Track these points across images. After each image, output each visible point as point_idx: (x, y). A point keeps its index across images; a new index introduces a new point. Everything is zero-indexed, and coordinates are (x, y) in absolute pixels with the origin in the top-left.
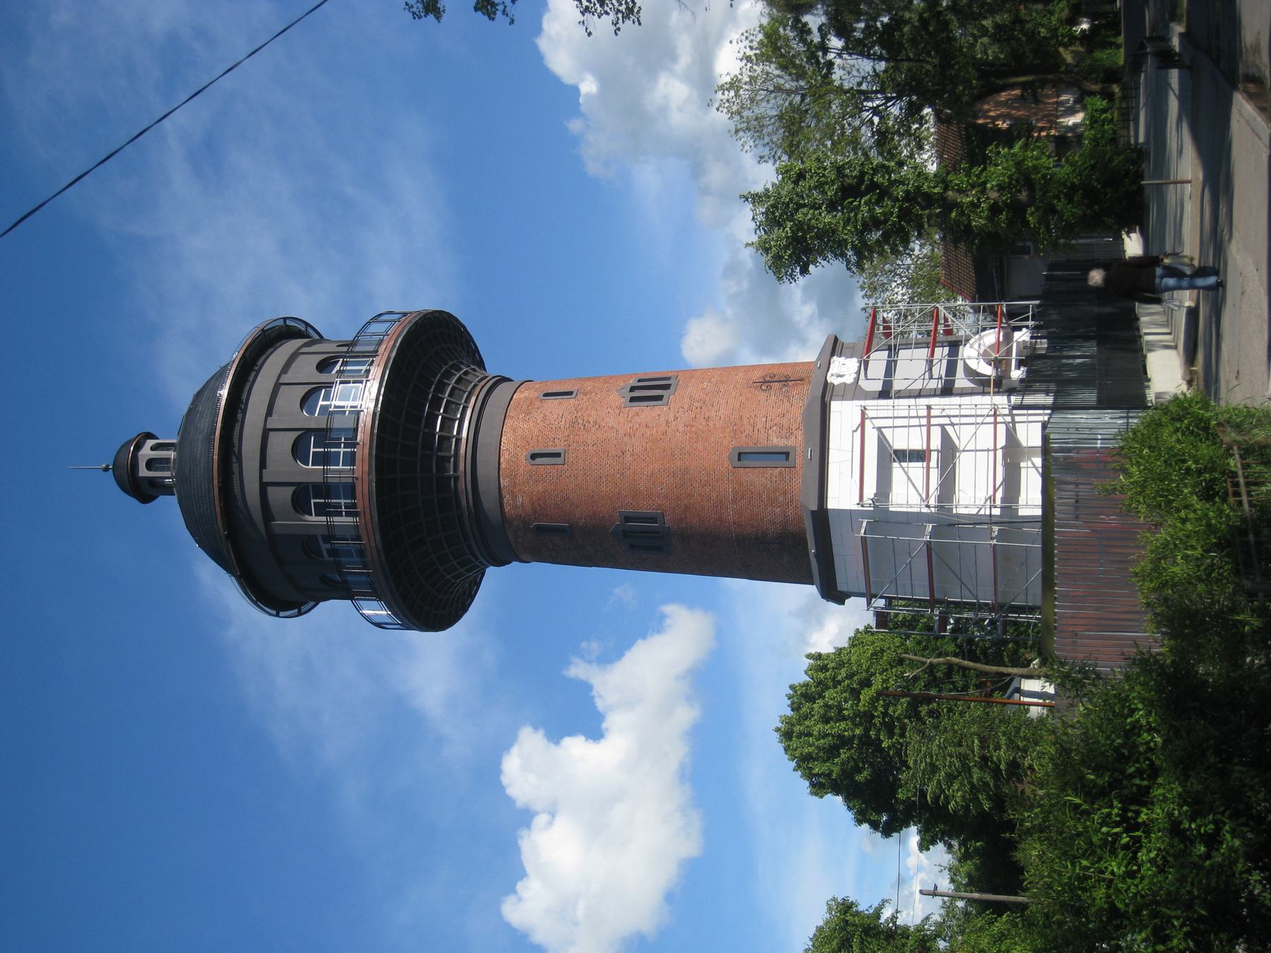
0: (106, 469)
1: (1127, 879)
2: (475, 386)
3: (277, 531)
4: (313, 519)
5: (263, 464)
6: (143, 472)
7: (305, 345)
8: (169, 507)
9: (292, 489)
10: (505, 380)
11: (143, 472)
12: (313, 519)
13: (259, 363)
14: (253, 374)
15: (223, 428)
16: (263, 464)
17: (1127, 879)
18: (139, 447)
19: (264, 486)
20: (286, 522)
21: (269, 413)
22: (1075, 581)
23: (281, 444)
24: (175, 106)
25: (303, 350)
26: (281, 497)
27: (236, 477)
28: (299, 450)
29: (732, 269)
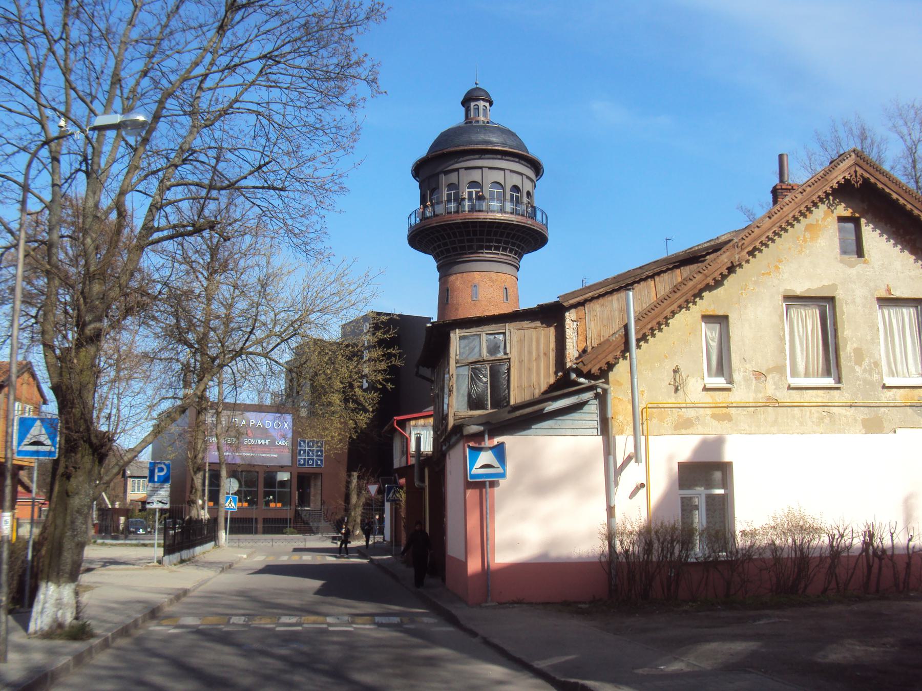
0: (476, 84)
1: (167, 485)
3: (440, 176)
4: (445, 193)
5: (467, 168)
6: (472, 104)
7: (528, 178)
8: (455, 117)
9: (457, 183)
10: (518, 270)
11: (472, 104)
12: (445, 193)
13: (507, 158)
14: (517, 160)
15: (498, 150)
16: (467, 168)
17: (167, 485)
18: (483, 100)
19: (457, 170)
20: (444, 180)
21: (512, 171)
22: (545, 354)
23: (476, 176)
24: (820, 392)
25: (524, 177)
26: (453, 178)
27: (472, 157)
28: (473, 184)
29: (463, 394)
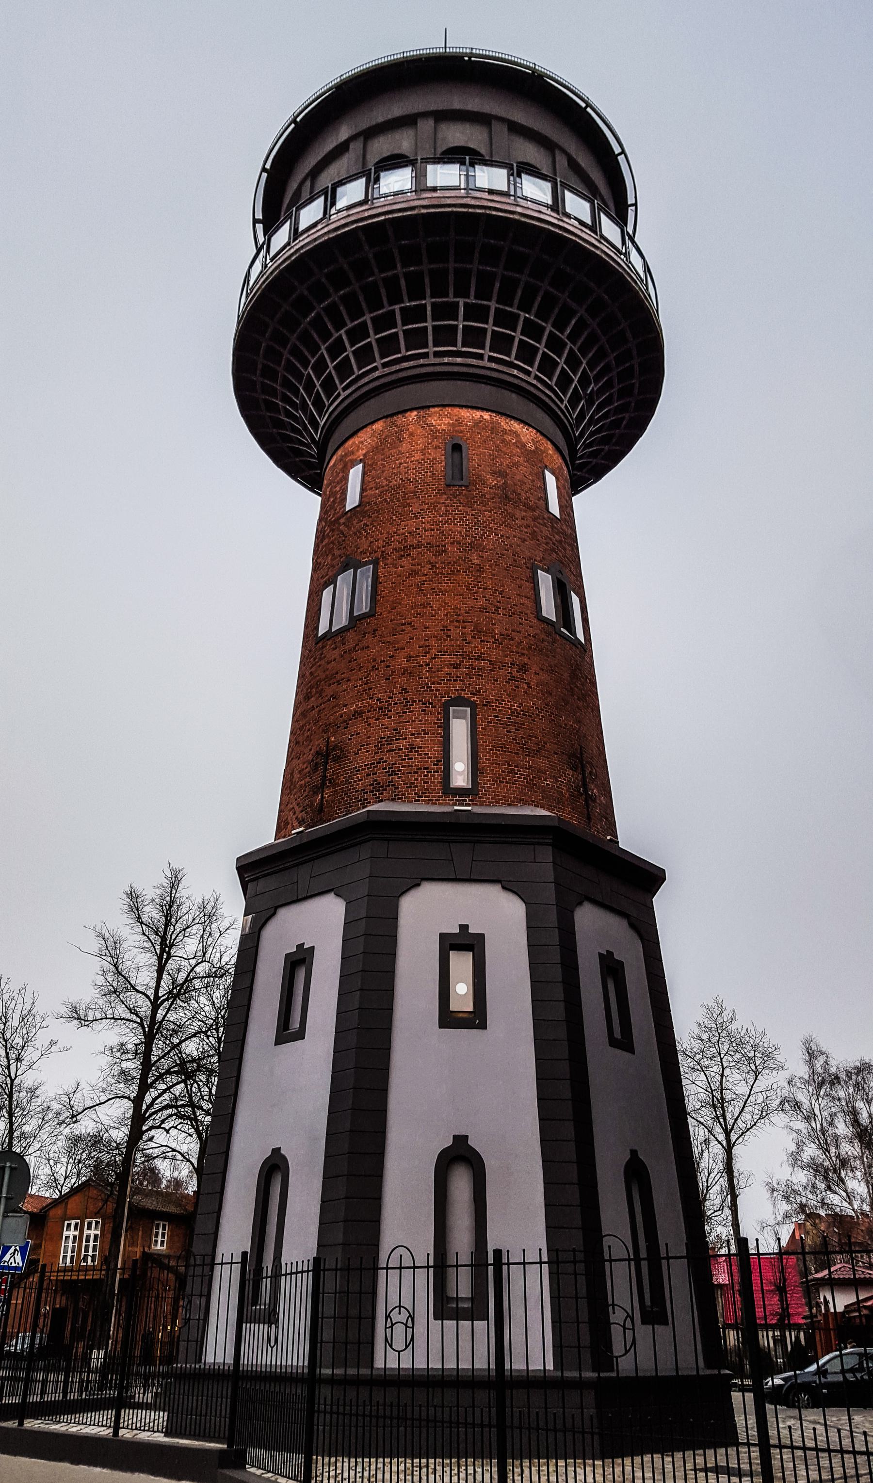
2: (528, 373)
